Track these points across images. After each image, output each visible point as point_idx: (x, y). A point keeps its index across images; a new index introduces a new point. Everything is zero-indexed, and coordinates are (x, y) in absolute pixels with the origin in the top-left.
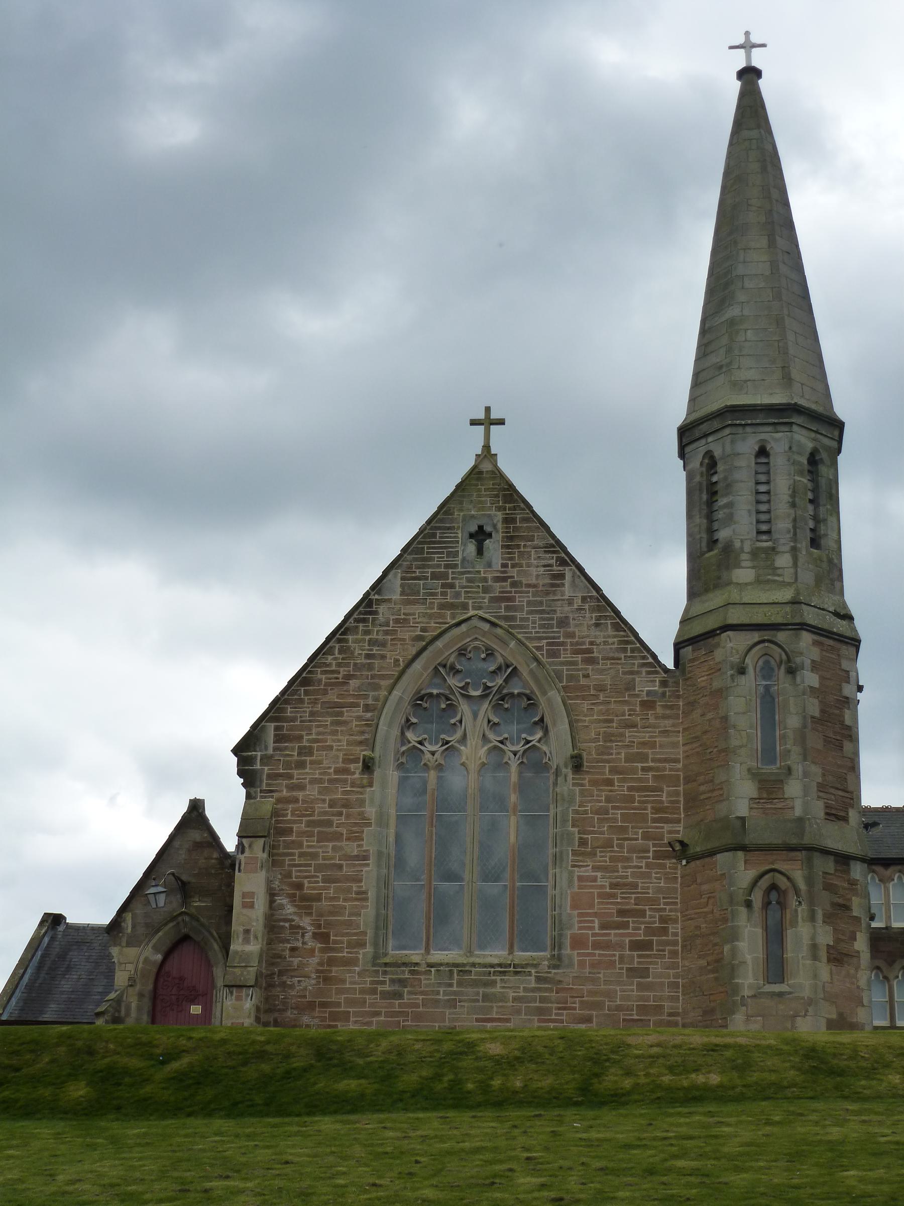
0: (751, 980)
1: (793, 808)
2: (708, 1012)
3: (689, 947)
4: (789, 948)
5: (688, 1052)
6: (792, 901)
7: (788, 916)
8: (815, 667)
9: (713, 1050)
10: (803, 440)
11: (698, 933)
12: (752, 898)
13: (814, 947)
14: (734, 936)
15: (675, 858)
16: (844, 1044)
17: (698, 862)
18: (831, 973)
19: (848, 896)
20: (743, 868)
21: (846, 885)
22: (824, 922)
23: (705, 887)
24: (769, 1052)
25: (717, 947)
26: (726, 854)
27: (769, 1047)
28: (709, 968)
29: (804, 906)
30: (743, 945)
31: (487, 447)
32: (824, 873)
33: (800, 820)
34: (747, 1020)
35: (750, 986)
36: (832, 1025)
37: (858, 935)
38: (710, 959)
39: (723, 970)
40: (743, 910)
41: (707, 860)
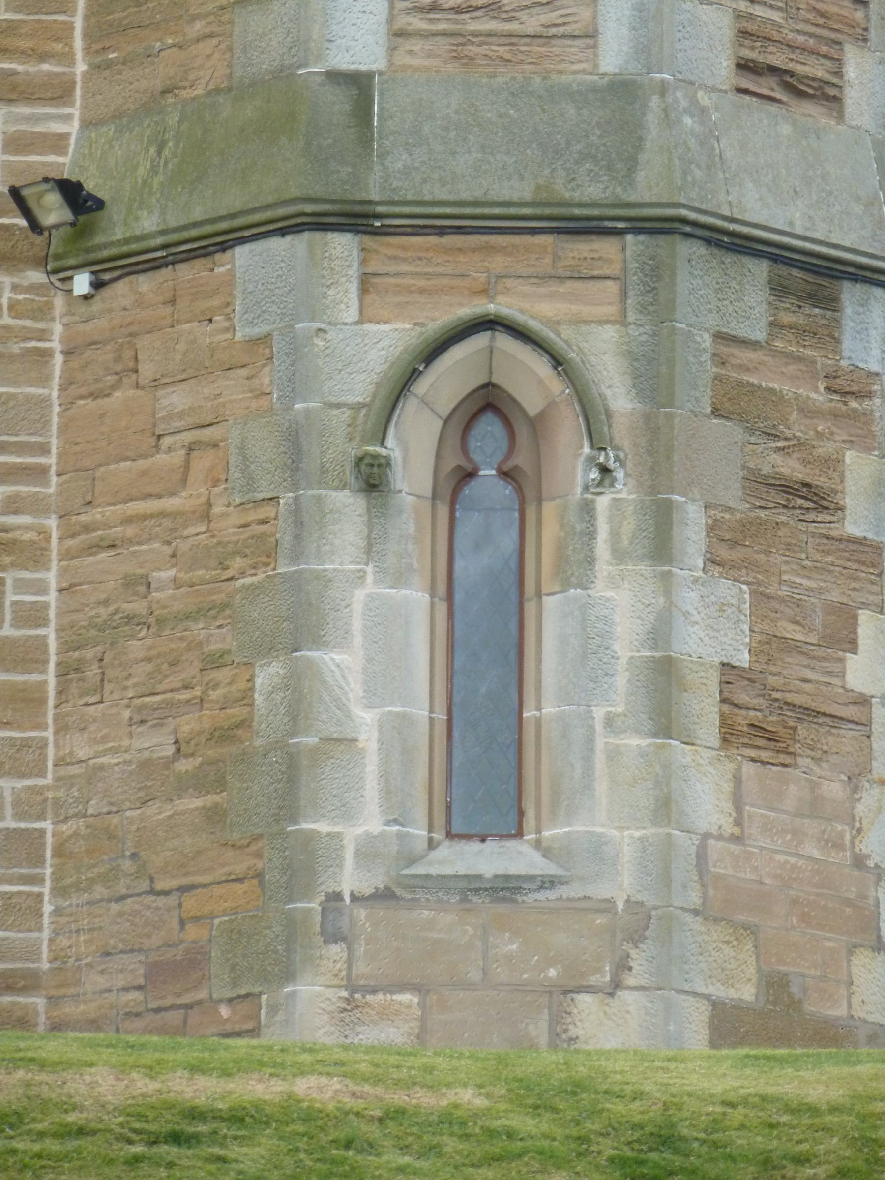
0: (371, 822)
1: (591, 35)
2: (175, 969)
3: (92, 673)
4: (549, 680)
5: (52, 1146)
6: (570, 462)
7: (550, 531)
9: (176, 1138)
11: (138, 607)
12: (392, 447)
13: (663, 676)
14: (301, 624)
15: (41, 262)
16: (814, 1110)
17: (145, 283)
19: (825, 448)
20: (352, 314)
21: (819, 397)
23: (177, 399)
24: (451, 1144)
25: (222, 675)
26: (277, 244)
27: (451, 1121)
28: (184, 766)
29: (624, 490)
30: (342, 663)
32: (719, 337)
33: (623, 94)
34: (350, 1006)
35: (368, 852)
36: (729, 1026)
38: (187, 724)
39: (248, 775)
40: (347, 504)
41: (186, 272)
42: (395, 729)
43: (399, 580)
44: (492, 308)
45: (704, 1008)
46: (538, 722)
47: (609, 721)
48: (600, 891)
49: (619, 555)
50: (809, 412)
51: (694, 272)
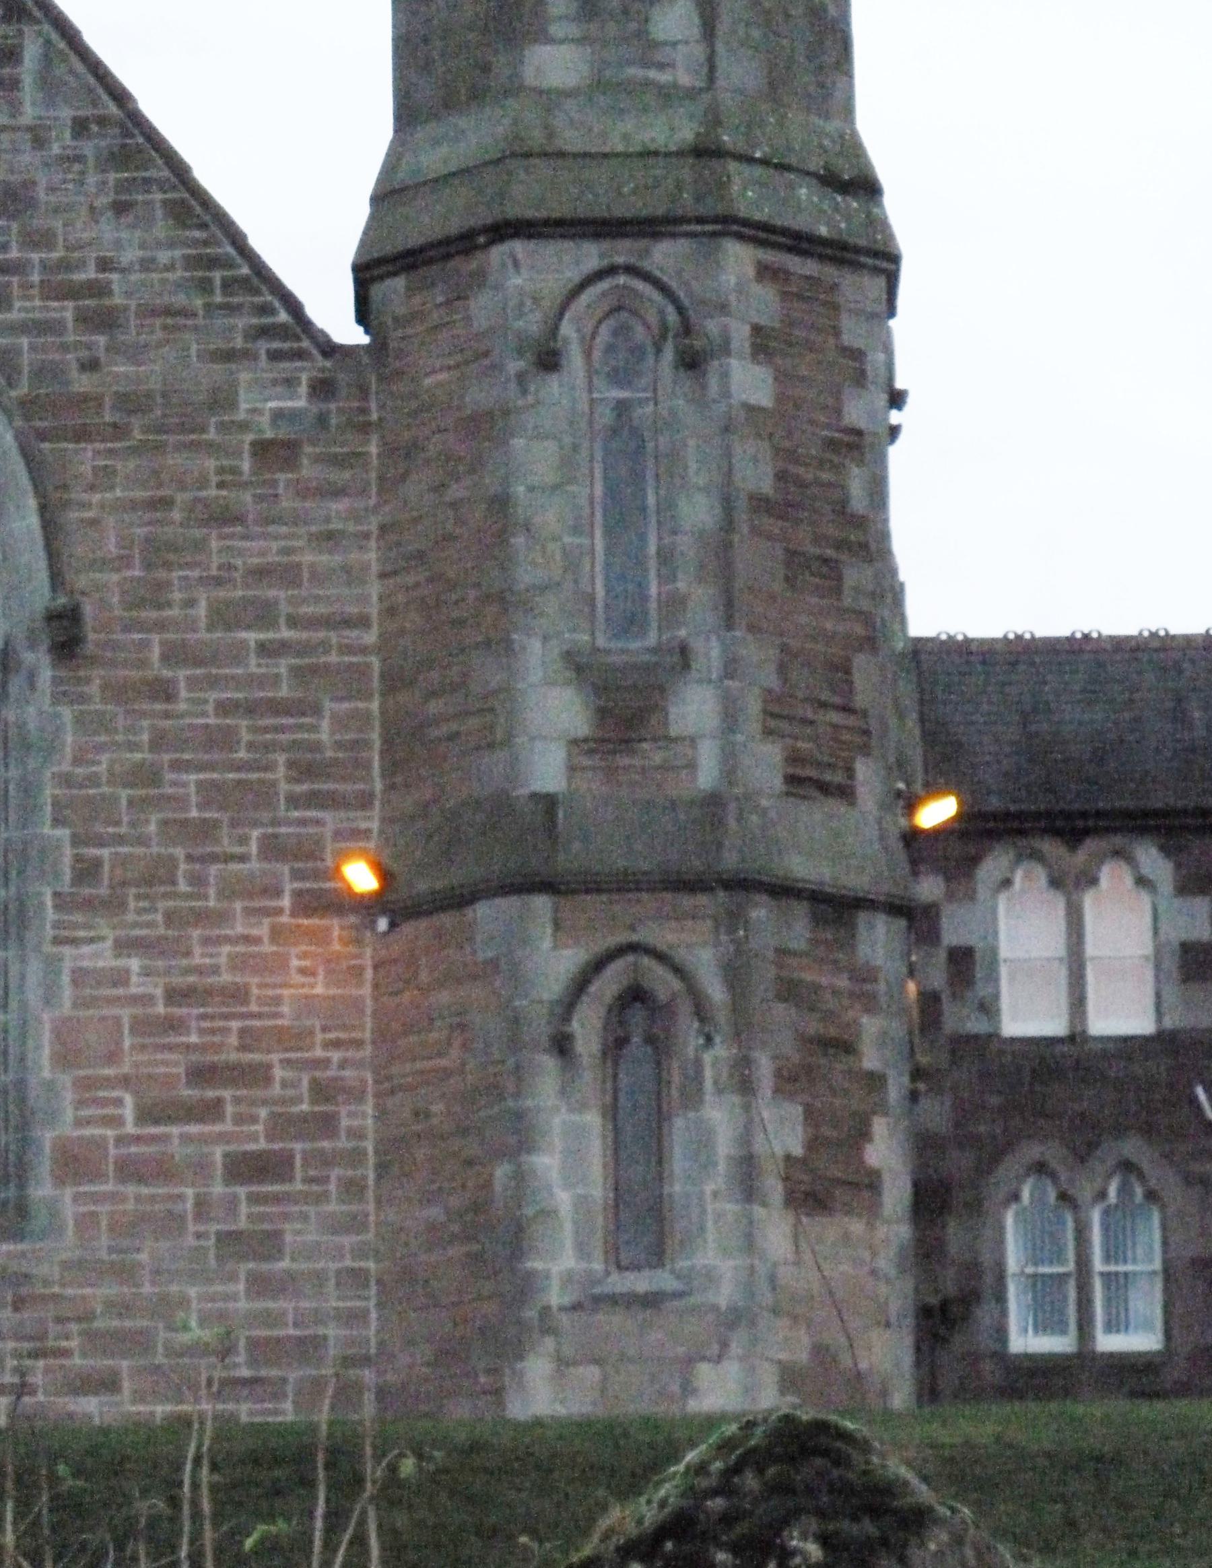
1: (692, 766)
8: (763, 344)
14: (521, 1136)
17: (423, 924)
21: (843, 982)
22: (777, 1091)
30: (547, 1163)
35: (568, 1278)
40: (549, 1062)
42: (581, 1203)
43: (583, 1107)
44: (635, 938)
45: (774, 1369)
46: (670, 1195)
47: (715, 1194)
48: (711, 1297)
49: (720, 1091)
50: (835, 992)
51: (761, 911)
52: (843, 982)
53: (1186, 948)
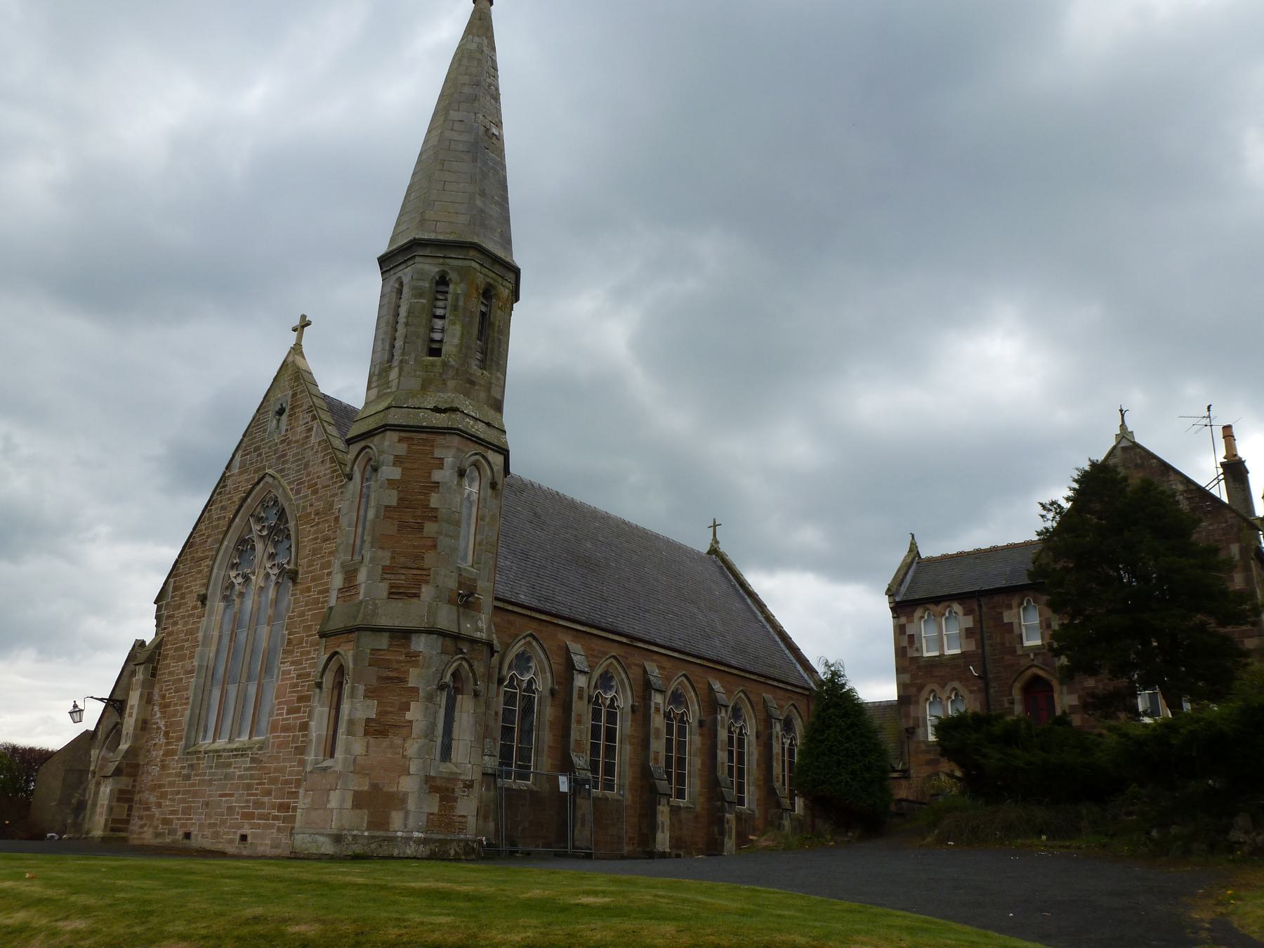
8: (398, 461)
10: (427, 267)
18: (367, 747)
22: (365, 696)
31: (297, 349)
37: (413, 705)
42: (319, 736)
50: (399, 662)
52: (402, 658)
53: (967, 629)
